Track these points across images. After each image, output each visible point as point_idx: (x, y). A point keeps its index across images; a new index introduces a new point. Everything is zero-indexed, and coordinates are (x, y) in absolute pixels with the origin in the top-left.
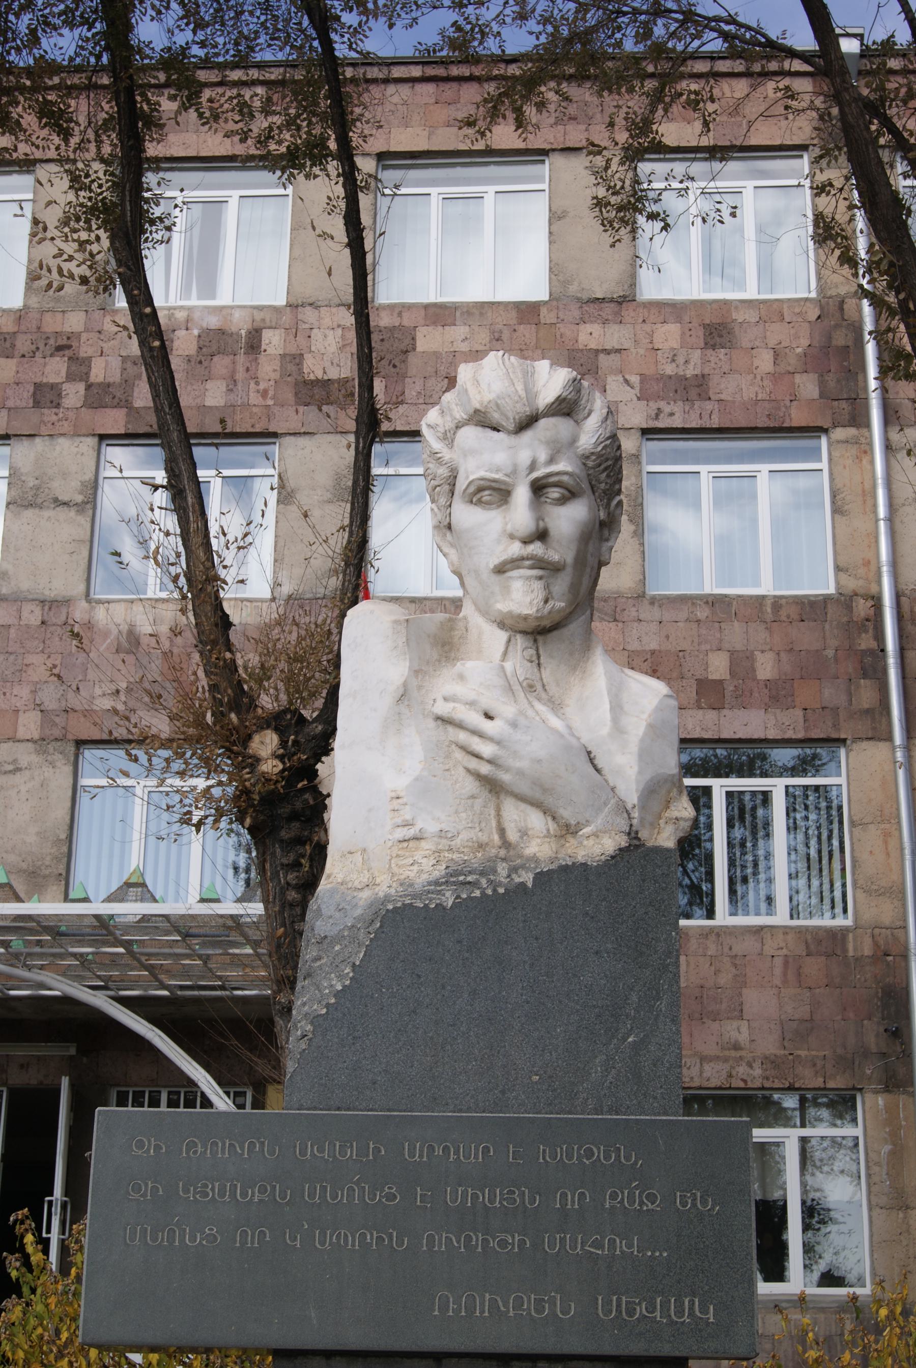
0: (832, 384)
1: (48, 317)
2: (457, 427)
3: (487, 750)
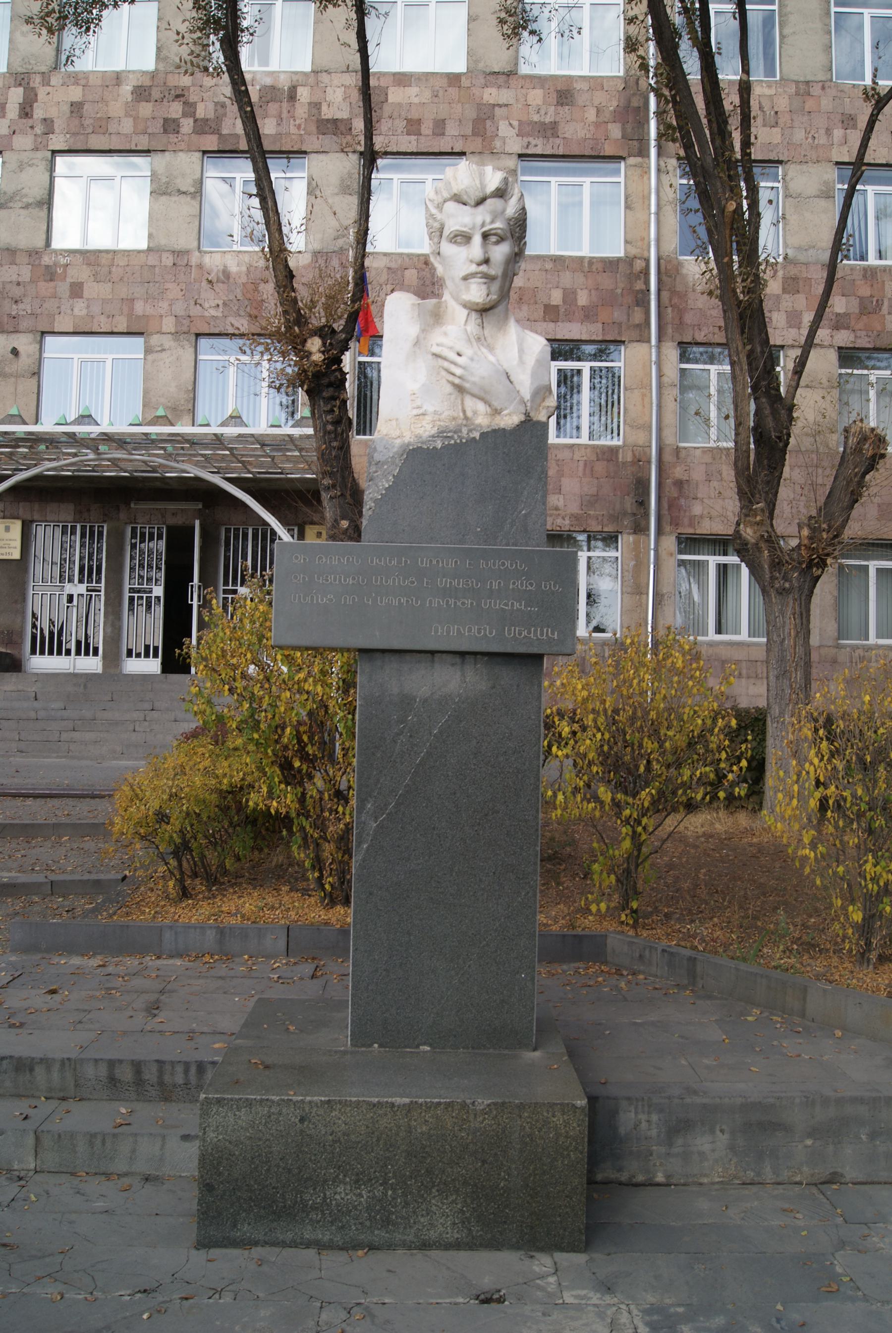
0: (629, 130)
1: (170, 76)
2: (444, 202)
3: (458, 371)
